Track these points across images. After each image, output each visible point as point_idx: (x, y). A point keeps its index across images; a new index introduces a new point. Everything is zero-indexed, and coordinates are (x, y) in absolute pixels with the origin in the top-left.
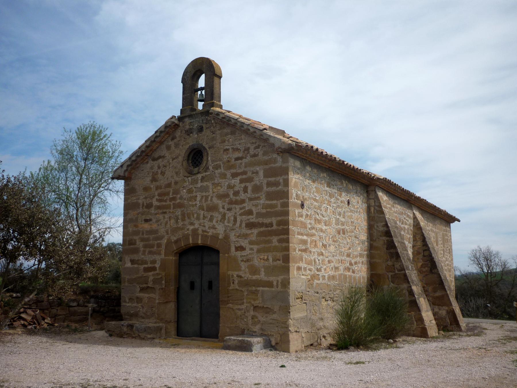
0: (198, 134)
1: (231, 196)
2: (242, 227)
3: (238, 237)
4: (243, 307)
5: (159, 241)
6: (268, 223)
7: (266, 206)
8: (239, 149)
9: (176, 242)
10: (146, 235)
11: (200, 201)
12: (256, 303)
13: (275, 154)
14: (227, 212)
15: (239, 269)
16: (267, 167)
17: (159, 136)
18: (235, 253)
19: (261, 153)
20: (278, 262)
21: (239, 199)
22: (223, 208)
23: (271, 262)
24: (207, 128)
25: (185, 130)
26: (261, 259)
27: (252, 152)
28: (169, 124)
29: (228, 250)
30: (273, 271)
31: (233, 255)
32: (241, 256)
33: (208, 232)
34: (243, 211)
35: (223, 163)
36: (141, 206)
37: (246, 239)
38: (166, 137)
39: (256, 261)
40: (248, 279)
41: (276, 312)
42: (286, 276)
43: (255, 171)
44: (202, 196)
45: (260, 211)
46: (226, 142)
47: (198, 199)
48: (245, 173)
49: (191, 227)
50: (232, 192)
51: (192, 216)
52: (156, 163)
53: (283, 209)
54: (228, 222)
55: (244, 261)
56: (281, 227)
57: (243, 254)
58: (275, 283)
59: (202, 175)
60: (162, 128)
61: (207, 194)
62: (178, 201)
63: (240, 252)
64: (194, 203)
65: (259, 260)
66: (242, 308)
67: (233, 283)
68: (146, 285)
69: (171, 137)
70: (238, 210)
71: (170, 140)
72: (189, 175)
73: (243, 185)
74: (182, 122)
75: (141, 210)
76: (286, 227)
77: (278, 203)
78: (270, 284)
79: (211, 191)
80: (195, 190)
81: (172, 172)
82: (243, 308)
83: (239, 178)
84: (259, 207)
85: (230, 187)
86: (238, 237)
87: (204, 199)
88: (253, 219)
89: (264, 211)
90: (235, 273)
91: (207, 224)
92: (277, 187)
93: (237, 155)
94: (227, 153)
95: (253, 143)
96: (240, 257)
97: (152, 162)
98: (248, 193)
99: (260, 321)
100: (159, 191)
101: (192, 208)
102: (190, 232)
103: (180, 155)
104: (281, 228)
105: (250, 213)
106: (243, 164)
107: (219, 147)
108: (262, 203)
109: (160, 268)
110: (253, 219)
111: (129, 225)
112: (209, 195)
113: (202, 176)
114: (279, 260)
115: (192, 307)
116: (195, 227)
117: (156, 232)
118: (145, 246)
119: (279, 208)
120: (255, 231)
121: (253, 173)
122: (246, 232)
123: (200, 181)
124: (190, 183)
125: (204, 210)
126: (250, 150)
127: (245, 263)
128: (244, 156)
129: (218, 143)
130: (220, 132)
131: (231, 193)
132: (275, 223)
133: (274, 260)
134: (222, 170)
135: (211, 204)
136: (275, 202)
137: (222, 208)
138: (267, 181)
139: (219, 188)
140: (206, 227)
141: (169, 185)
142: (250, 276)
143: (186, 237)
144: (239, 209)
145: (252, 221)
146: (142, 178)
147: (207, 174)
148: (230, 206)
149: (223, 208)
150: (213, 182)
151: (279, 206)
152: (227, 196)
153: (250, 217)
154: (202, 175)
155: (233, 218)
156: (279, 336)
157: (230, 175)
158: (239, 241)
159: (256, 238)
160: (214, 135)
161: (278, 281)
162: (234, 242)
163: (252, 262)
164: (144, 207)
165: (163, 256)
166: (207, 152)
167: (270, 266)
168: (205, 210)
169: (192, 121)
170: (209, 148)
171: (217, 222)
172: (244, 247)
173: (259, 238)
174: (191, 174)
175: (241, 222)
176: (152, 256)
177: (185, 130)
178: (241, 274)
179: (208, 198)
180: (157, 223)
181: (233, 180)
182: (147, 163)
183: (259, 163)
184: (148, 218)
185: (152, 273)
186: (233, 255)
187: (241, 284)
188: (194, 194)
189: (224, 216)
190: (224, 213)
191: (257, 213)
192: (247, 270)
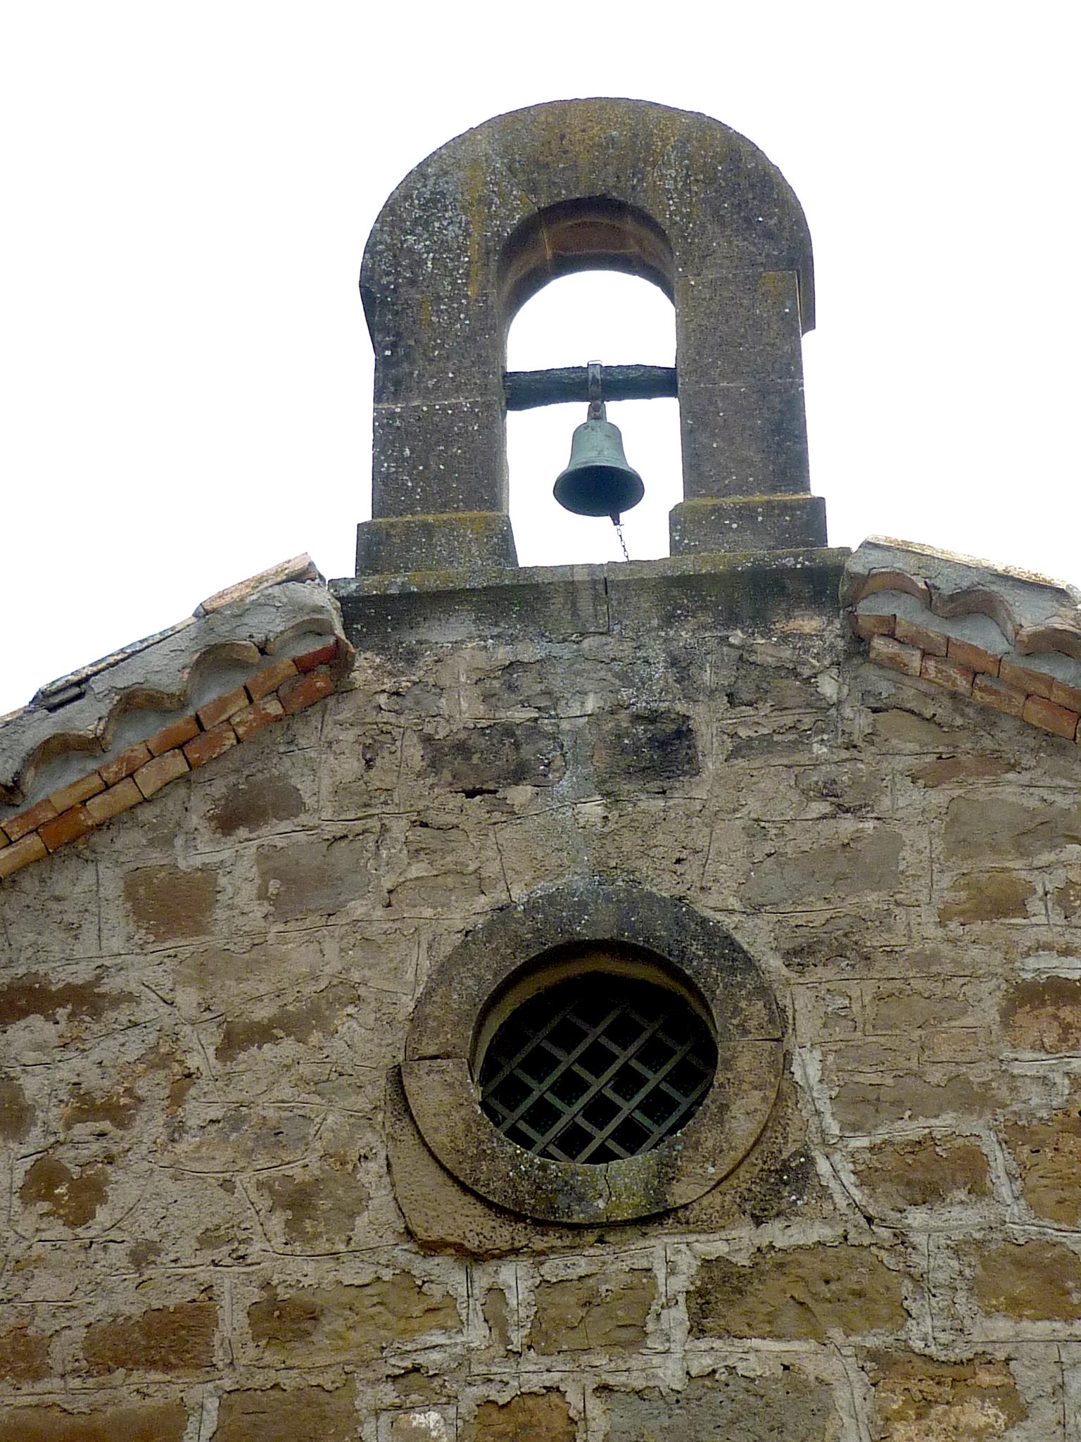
17: (92, 746)
25: (427, 740)
28: (269, 625)
38: (149, 779)
46: (1035, 905)
59: (715, 1247)
60: (155, 658)
69: (219, 788)
72: (504, 1234)
74: (381, 650)
81: (227, 1186)
103: (356, 1000)
107: (935, 957)
113: (707, 1263)
123: (678, 1316)
124: (517, 1338)
129: (928, 917)
130: (938, 798)
139: (979, 1420)
147: (777, 1234)
160: (847, 825)
169: (530, 651)
174: (542, 1225)
177: (427, 740)
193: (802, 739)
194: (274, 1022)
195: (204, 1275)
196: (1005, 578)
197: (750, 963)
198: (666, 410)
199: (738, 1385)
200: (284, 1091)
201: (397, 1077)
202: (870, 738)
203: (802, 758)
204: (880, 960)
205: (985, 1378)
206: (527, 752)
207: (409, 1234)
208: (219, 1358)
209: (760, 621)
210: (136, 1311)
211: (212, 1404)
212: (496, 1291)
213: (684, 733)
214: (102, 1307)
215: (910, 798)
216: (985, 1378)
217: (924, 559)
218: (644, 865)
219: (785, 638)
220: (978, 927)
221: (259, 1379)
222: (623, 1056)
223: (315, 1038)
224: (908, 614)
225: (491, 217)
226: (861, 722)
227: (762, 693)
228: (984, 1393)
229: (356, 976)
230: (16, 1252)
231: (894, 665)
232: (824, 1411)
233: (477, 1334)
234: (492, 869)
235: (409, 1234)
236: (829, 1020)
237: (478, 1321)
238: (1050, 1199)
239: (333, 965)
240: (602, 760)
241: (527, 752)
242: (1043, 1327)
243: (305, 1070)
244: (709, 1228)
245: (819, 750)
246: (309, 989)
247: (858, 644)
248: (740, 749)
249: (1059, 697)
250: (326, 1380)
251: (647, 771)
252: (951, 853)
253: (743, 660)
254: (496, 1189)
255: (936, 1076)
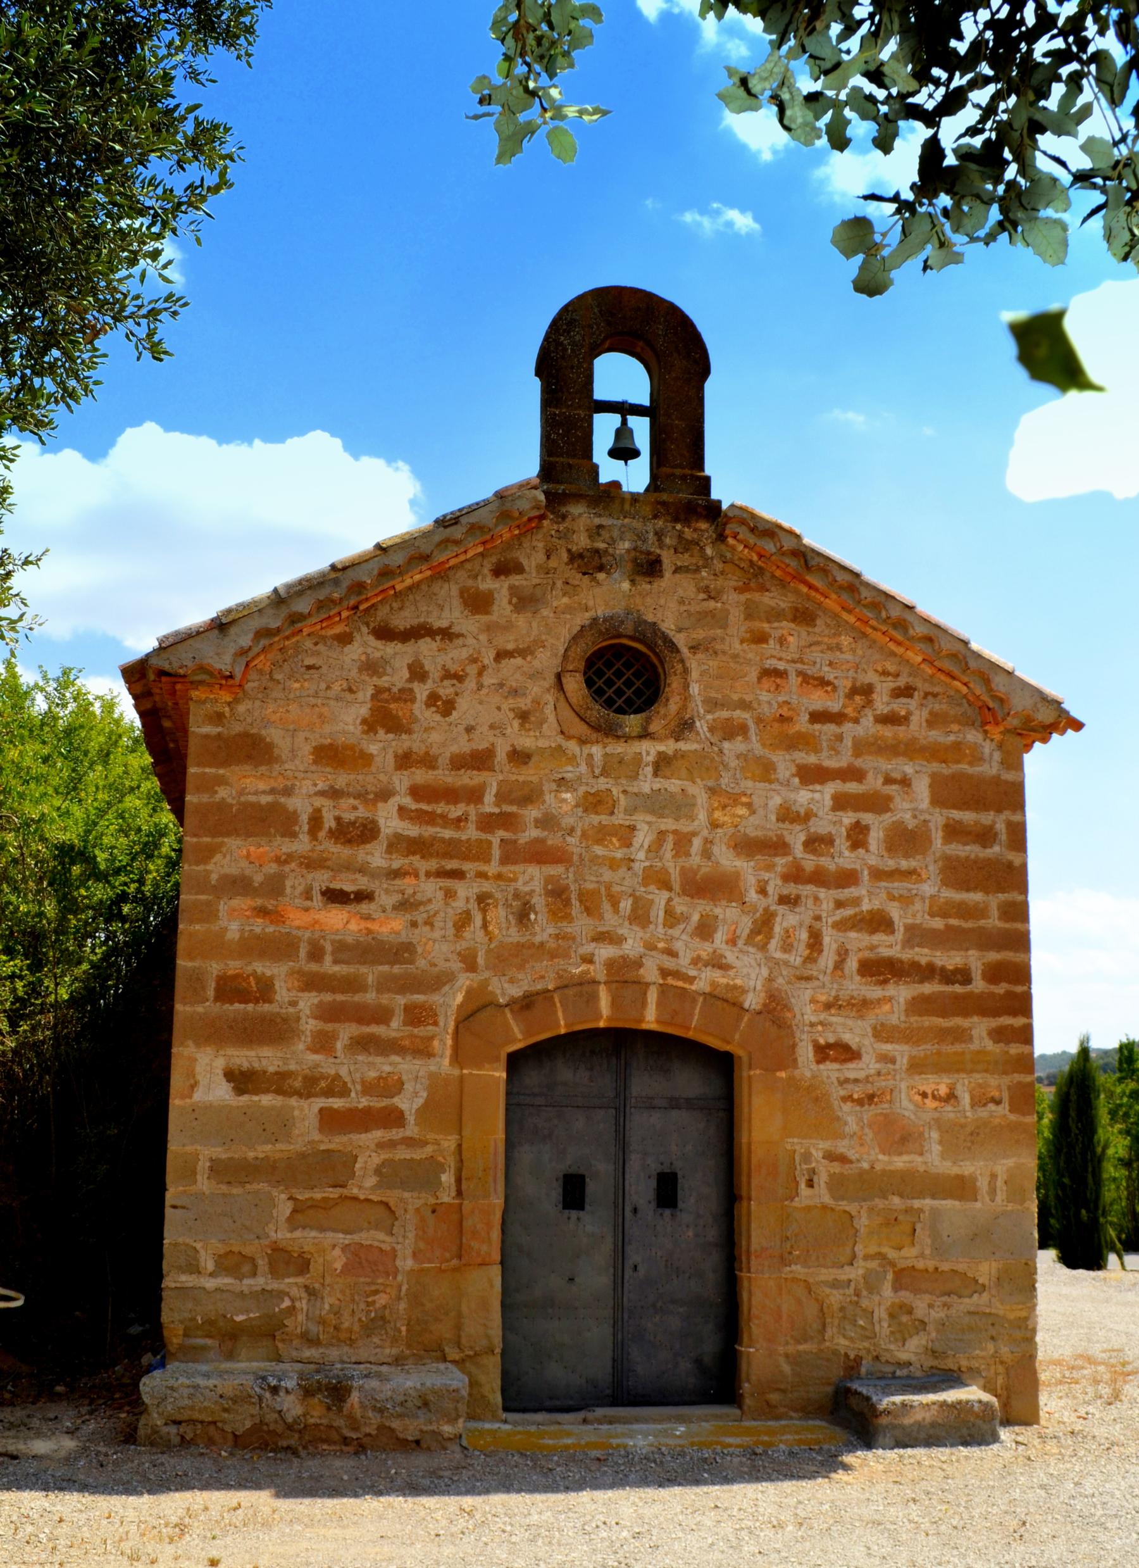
0: (633, 582)
1: (798, 850)
2: (847, 971)
3: (828, 1006)
4: (855, 1273)
5: (419, 998)
6: (951, 968)
7: (942, 911)
8: (829, 683)
9: (526, 1004)
10: (336, 962)
11: (649, 850)
12: (906, 1258)
13: (974, 732)
14: (781, 909)
15: (829, 1124)
16: (945, 770)
18: (814, 1066)
19: (919, 718)
20: (992, 1107)
21: (832, 867)
22: (763, 891)
23: (968, 1107)
24: (677, 570)
26: (924, 1095)
27: (882, 703)
29: (787, 1058)
30: (973, 1142)
31: (808, 1074)
32: (843, 1082)
33: (691, 979)
34: (849, 912)
35: (759, 721)
36: (306, 828)
37: (862, 1017)
39: (905, 1103)
40: (873, 1168)
41: (984, 1286)
42: (1023, 1161)
43: (897, 775)
44: (662, 834)
45: (918, 922)
46: (771, 642)
47: (643, 837)
48: (853, 774)
49: (605, 952)
50: (802, 837)
51: (606, 906)
52: (399, 655)
53: (1007, 926)
54: (787, 947)
55: (853, 1101)
56: (1001, 989)
57: (852, 1075)
58: (983, 1184)
59: (661, 748)
61: (684, 827)
62: (534, 833)
63: (836, 1066)
64: (619, 855)
65: (918, 1098)
66: (844, 1277)
67: (810, 1184)
68: (339, 1190)
70: (827, 905)
71: (486, 571)
73: (848, 818)
75: (302, 844)
76: (1019, 989)
77: (994, 901)
78: (962, 1188)
79: (702, 816)
80: (623, 801)
82: (852, 1276)
83: (831, 789)
84: (918, 906)
85: (787, 815)
86: (828, 1006)
87: (669, 845)
88: (891, 946)
89: (938, 923)
90: (818, 1148)
91: (687, 947)
92: (985, 847)
93: (818, 700)
94: (778, 686)
95: (885, 673)
96: (836, 1084)
97: (371, 640)
98: (867, 851)
99: (923, 1322)
100: (421, 776)
101: (607, 875)
102: (598, 971)
104: (1002, 991)
105: (879, 922)
106: (848, 742)
108: (928, 895)
109: (423, 1112)
110: (891, 946)
111: (222, 907)
112: (694, 834)
113: (659, 753)
114: (998, 1102)
115: (571, 1280)
116: (621, 953)
117: (402, 952)
118: (331, 1014)
119: (994, 921)
120: (902, 992)
121: (889, 781)
122: (863, 992)
125: (670, 889)
126: (875, 696)
127: (858, 1108)
128: (849, 711)
131: (797, 838)
132: (980, 972)
133: (979, 1101)
134: (755, 744)
135: (704, 870)
136: (976, 897)
137: (757, 892)
138: (948, 818)
140: (681, 954)
141: (481, 760)
142: (881, 1157)
143: (585, 987)
144: (832, 905)
145: (885, 952)
146: (313, 701)
147: (683, 746)
148: (791, 889)
149: (763, 891)
150: (711, 783)
151: (995, 913)
152: (779, 847)
153: (879, 938)
154: (661, 748)
155: (804, 935)
156: (1001, 1369)
157: (794, 770)
158: (831, 1024)
159: (903, 1018)
161: (994, 1176)
162: (812, 1025)
163: (886, 1106)
164: (322, 834)
165: (443, 1064)
166: (682, 661)
167: (963, 1120)
168: (677, 887)
169: (605, 521)
170: (694, 649)
171: (732, 942)
172: (854, 1047)
173: (919, 1019)
175: (843, 955)
176: (379, 1060)
177: (569, 551)
178: (842, 1150)
179: (690, 841)
180: (408, 917)
181: (803, 793)
182: (345, 639)
183: (910, 750)
184: (349, 888)
185: (378, 1134)
186: (808, 1074)
187: (837, 1185)
188: (619, 819)
189: (764, 925)
190: (766, 910)
191: (910, 928)
192: (869, 1134)
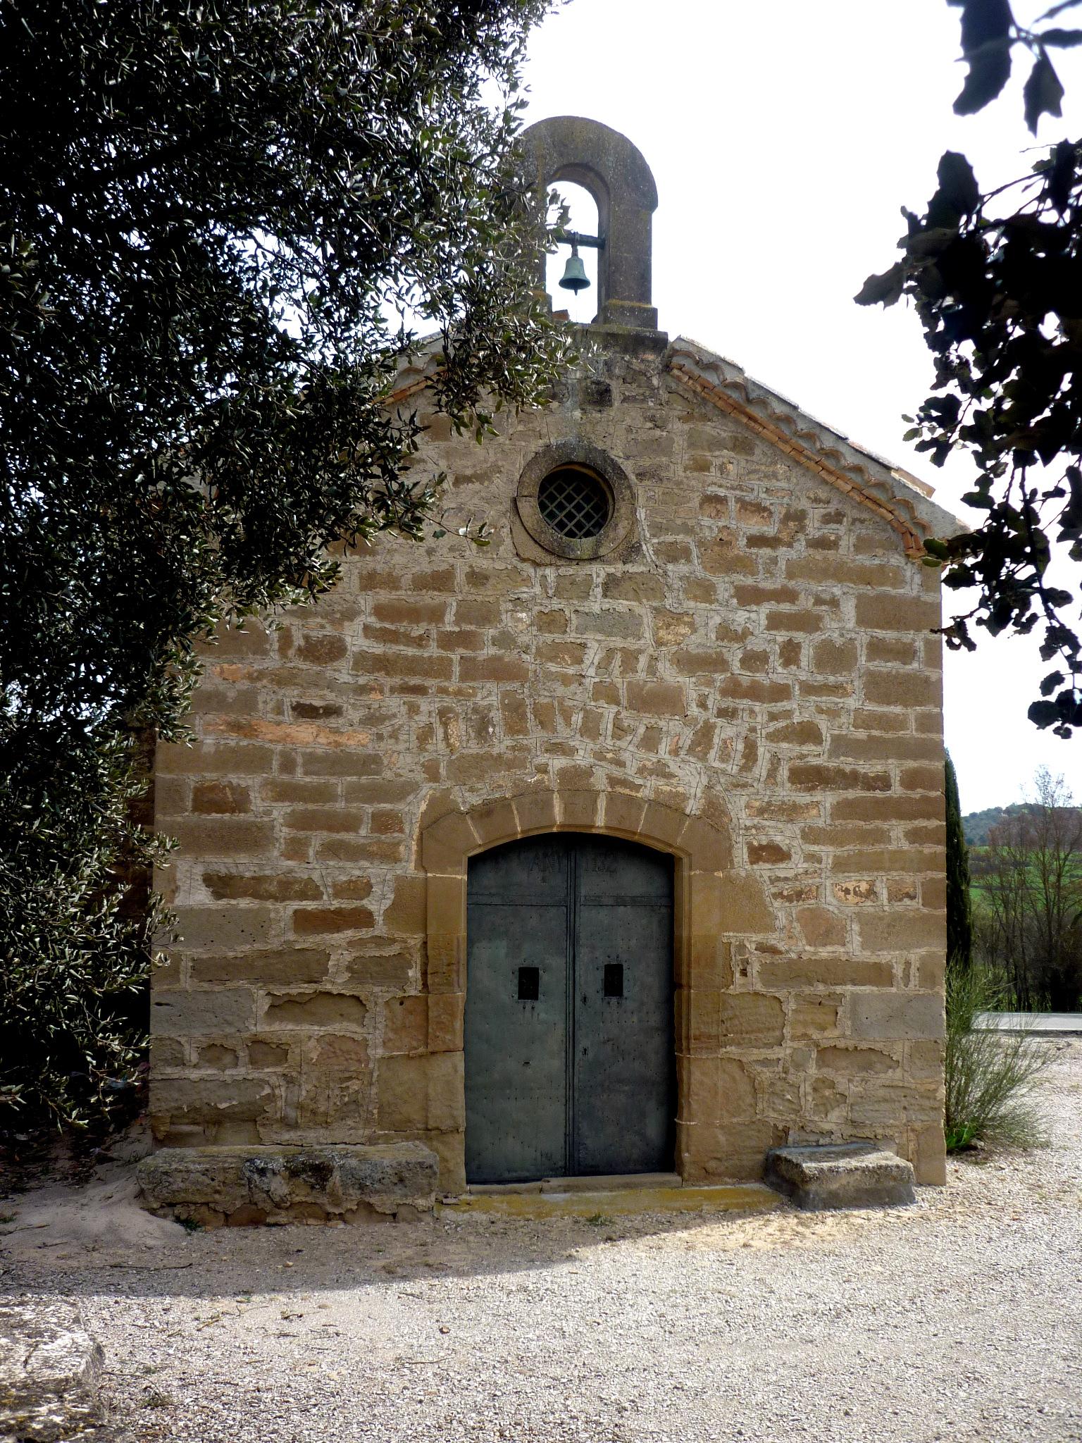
46: (712, 469)
59: (611, 570)
72: (548, 558)
103: (500, 472)
107: (681, 482)
113: (608, 574)
123: (599, 590)
124: (551, 592)
130: (686, 427)
147: (630, 568)
160: (658, 432)
193: (644, 401)
194: (472, 476)
195: (451, 561)
196: (724, 361)
197: (626, 477)
198: (594, 251)
199: (616, 615)
200: (476, 501)
201: (514, 501)
202: (667, 403)
203: (644, 406)
204: (665, 482)
205: (686, 619)
206: (556, 389)
207: (517, 555)
208: (456, 589)
209: (635, 353)
210: (429, 571)
211: (454, 604)
212: (544, 577)
213: (607, 391)
214: (418, 568)
215: (678, 426)
216: (686, 619)
217: (700, 350)
218: (593, 436)
219: (642, 361)
220: (696, 474)
221: (470, 598)
222: (578, 499)
223: (486, 483)
224: (689, 365)
225: (546, 164)
226: (664, 396)
227: (634, 380)
228: (685, 623)
229: (500, 463)
230: (388, 546)
231: (678, 379)
232: (640, 624)
233: (537, 590)
234: (544, 431)
235: (517, 555)
236: (649, 499)
237: (538, 585)
238: (708, 566)
239: (492, 458)
240: (580, 397)
241: (556, 389)
242: (703, 605)
243: (483, 494)
244: (609, 563)
245: (651, 404)
246: (485, 466)
247: (667, 368)
248: (626, 399)
249: (731, 401)
250: (491, 599)
251: (596, 403)
252: (689, 447)
253: (628, 366)
254: (545, 543)
255: (679, 522)
